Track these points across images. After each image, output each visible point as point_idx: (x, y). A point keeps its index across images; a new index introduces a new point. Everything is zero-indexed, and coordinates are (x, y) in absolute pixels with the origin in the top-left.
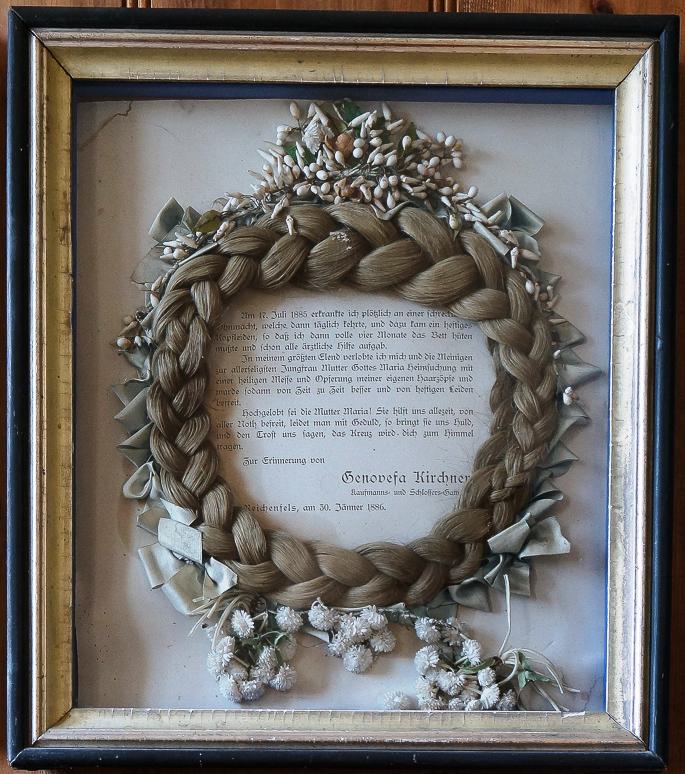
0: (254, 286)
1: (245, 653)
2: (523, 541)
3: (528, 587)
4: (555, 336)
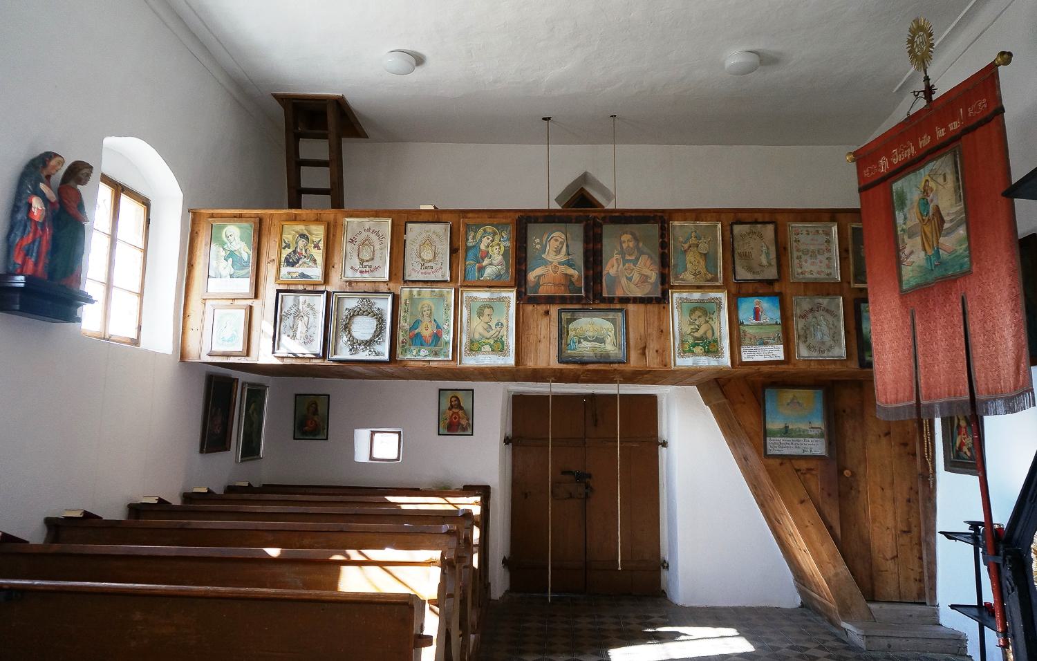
0: (353, 315)
1: (351, 350)
2: (13, 312)
3: (319, 255)
4: (382, 320)
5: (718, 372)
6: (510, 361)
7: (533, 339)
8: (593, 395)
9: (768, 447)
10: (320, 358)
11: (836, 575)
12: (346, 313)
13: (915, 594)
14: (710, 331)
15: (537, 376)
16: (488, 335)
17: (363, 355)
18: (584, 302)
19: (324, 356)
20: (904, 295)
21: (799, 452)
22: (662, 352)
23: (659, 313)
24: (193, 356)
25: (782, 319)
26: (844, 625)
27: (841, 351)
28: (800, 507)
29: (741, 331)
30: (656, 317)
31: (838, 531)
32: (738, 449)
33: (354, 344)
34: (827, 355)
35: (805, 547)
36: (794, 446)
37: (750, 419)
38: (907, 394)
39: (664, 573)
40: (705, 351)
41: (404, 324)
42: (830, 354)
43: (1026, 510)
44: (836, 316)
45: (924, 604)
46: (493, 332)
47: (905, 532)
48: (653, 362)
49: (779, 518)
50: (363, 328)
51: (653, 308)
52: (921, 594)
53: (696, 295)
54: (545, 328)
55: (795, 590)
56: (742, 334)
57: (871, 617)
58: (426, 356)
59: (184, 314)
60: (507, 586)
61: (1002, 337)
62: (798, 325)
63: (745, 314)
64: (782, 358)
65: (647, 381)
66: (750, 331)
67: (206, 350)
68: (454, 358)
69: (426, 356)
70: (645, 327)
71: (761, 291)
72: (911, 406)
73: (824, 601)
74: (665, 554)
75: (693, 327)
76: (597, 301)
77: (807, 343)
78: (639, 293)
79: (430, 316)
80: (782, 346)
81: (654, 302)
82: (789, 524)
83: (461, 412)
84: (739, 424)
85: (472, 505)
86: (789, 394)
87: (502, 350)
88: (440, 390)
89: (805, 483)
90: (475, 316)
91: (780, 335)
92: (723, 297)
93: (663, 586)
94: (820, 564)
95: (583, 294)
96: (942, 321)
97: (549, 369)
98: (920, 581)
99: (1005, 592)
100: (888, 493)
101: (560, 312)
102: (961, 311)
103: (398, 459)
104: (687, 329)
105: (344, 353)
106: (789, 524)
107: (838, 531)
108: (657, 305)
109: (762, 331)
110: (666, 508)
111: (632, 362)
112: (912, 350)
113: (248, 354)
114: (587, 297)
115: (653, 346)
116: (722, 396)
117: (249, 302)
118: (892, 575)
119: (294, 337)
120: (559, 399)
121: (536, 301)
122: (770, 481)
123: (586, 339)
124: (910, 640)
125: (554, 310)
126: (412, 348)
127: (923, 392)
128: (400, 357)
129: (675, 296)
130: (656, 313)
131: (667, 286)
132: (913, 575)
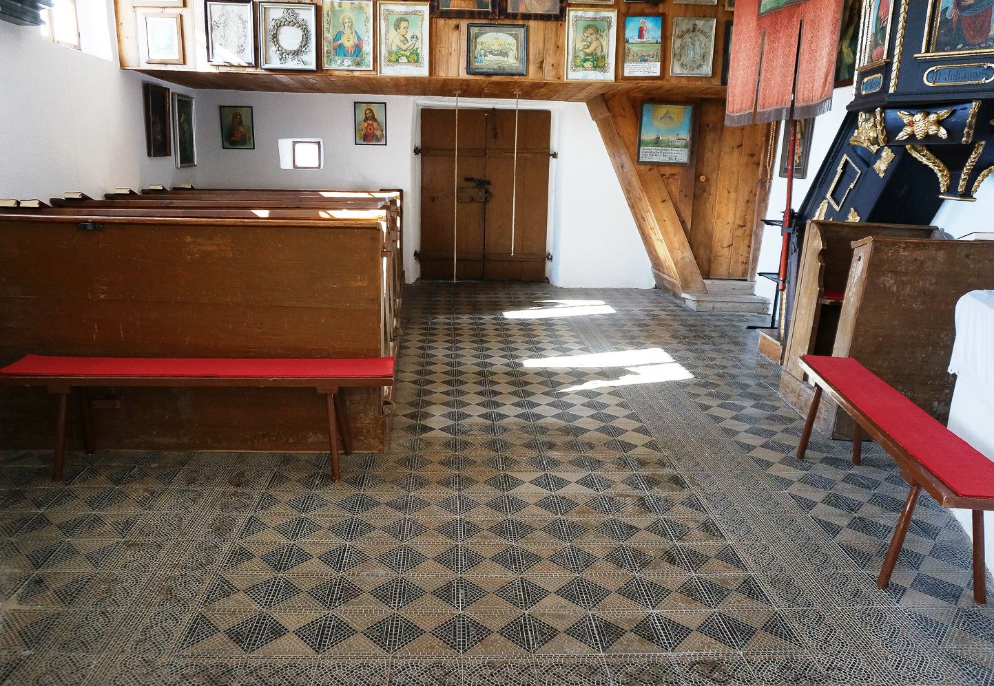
1: (280, 59)
5: (604, 87)
6: (423, 71)
7: (444, 51)
8: (494, 110)
9: (641, 155)
10: (253, 67)
11: (683, 258)
12: (273, 23)
13: (740, 274)
14: (600, 47)
15: (445, 88)
16: (404, 47)
17: (292, 64)
18: (490, 17)
19: (256, 65)
20: (760, 17)
21: (666, 160)
22: (557, 66)
23: (557, 30)
24: (132, 64)
25: (662, 38)
26: (684, 295)
27: (707, 69)
28: (661, 205)
29: (626, 49)
30: (554, 34)
31: (689, 226)
32: (617, 157)
33: (283, 54)
34: (696, 73)
35: (661, 237)
36: (662, 154)
37: (627, 130)
38: (749, 104)
39: (548, 264)
40: (594, 67)
41: (328, 35)
42: (699, 72)
43: (816, 192)
44: (708, 37)
45: (746, 280)
46: (408, 45)
47: (741, 226)
48: (549, 76)
49: (643, 214)
50: (290, 38)
51: (551, 25)
52: (745, 273)
53: (590, 14)
54: (454, 41)
55: (652, 275)
56: (627, 51)
57: (705, 290)
58: (349, 66)
59: (117, 21)
60: (418, 275)
61: (821, 55)
62: (676, 44)
63: (631, 33)
64: (658, 74)
65: (543, 95)
66: (634, 49)
67: (144, 58)
68: (374, 69)
69: (349, 66)
70: (544, 43)
71: (647, 11)
72: (750, 113)
73: (672, 280)
74: (550, 248)
75: (585, 43)
76: (502, 17)
77: (681, 61)
78: (539, 10)
79: (351, 28)
80: (659, 63)
81: (553, 19)
82: (651, 220)
83: (375, 124)
84: (619, 135)
85: (377, 215)
86: (664, 109)
87: (417, 61)
88: (355, 103)
89: (667, 186)
90: (392, 28)
91: (659, 54)
92: (613, 15)
93: (547, 275)
94: (671, 250)
95: (490, 9)
96: (783, 41)
97: (458, 80)
98: (746, 263)
99: (790, 252)
100: (733, 195)
101: (469, 27)
102: (798, 33)
103: (319, 167)
104: (580, 46)
105: (275, 63)
106: (651, 220)
107: (689, 226)
108: (555, 22)
109: (644, 49)
110: (552, 236)
111: (530, 75)
112: (758, 67)
113: (185, 63)
114: (493, 12)
115: (549, 60)
116: (606, 110)
117: (179, 11)
118: (725, 259)
119: (226, 46)
120: (466, 113)
121: (448, 15)
122: (640, 185)
123: (491, 53)
124: (730, 304)
125: (464, 24)
126: (337, 58)
127: (760, 101)
128: (326, 66)
129: (572, 14)
130: (554, 28)
131: (565, 4)
132: (742, 259)
